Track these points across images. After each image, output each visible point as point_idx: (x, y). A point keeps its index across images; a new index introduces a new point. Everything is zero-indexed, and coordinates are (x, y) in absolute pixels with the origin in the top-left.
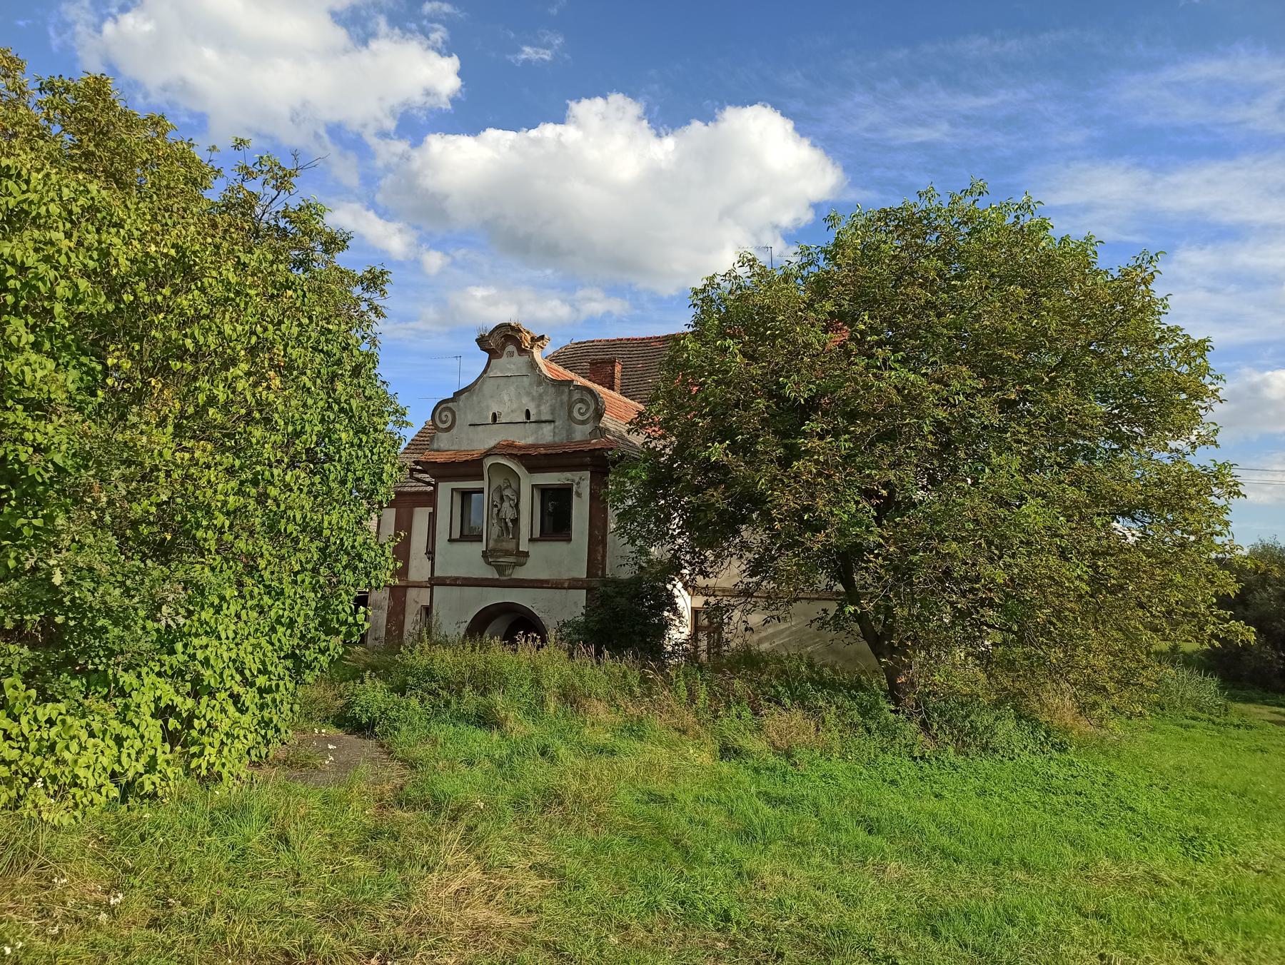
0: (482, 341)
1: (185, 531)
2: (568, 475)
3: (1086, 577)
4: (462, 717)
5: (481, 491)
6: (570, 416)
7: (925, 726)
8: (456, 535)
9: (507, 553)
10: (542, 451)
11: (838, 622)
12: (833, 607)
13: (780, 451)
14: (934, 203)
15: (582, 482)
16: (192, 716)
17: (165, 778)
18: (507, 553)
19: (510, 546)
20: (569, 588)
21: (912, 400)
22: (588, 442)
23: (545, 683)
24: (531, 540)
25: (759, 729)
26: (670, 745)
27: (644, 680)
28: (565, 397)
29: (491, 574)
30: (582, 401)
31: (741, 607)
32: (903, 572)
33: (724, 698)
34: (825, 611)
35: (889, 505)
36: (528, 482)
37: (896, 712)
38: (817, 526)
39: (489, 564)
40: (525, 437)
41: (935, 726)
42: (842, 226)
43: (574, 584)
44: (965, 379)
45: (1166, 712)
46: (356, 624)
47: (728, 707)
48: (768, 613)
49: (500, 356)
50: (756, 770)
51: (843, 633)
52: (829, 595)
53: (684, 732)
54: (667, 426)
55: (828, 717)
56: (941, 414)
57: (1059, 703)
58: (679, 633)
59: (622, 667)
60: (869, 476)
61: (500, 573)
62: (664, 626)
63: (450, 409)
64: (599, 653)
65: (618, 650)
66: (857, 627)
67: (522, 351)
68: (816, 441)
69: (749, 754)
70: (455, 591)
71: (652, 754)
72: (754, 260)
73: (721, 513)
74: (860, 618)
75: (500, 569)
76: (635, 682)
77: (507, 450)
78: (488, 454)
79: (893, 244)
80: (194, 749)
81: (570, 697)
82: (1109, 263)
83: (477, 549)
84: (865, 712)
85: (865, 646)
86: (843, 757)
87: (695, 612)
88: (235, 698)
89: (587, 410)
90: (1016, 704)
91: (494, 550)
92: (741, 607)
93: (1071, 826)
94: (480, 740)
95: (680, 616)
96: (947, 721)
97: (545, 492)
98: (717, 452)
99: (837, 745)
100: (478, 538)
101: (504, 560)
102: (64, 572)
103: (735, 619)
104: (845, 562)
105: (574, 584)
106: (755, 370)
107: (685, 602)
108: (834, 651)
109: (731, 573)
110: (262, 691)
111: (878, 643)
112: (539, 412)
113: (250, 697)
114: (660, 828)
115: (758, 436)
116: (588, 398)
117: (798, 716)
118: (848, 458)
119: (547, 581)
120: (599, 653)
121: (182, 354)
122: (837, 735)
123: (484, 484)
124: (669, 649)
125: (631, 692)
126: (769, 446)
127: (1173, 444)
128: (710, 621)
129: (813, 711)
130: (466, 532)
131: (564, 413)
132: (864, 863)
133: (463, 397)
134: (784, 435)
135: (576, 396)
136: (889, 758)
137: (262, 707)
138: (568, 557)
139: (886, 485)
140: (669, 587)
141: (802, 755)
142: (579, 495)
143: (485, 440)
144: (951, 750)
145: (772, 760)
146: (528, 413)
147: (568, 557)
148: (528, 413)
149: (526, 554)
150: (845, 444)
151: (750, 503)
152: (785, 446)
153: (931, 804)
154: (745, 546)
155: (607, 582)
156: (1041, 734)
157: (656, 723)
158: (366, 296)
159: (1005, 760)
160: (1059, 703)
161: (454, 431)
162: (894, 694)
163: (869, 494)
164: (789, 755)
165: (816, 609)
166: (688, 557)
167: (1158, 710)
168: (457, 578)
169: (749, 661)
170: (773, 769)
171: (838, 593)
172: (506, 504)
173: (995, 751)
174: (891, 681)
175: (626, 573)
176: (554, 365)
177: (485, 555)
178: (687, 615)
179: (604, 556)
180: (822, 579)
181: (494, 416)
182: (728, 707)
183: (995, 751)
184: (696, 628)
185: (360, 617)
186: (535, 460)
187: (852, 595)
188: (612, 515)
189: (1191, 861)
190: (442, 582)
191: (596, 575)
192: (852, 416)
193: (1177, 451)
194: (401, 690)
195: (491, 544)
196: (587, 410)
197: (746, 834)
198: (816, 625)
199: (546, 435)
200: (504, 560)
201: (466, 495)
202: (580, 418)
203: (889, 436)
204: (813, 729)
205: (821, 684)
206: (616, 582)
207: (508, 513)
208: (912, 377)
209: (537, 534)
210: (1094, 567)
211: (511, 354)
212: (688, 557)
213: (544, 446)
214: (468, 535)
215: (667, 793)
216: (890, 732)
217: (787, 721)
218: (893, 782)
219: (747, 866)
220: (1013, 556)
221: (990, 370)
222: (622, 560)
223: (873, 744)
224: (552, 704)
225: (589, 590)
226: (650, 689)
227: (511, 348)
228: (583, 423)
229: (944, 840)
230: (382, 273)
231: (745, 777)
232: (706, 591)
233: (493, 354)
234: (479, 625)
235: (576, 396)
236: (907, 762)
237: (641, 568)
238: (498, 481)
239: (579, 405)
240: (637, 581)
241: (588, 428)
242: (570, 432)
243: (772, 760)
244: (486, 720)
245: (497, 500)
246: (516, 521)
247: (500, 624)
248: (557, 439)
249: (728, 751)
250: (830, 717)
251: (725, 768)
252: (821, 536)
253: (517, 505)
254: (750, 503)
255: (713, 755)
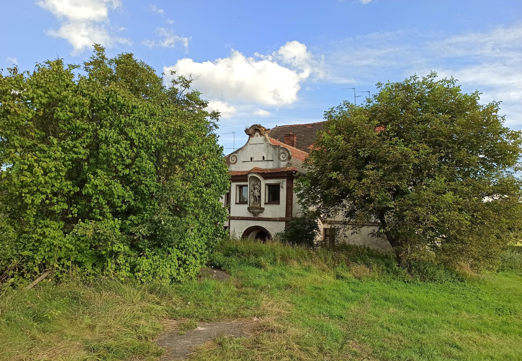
0: (247, 131)
1: (183, 209)
2: (279, 180)
3: (469, 219)
4: (251, 264)
5: (247, 186)
6: (279, 159)
7: (409, 271)
8: (238, 201)
9: (257, 208)
10: (269, 171)
11: (379, 235)
12: (376, 229)
13: (357, 175)
14: (417, 80)
15: (284, 184)
16: (185, 260)
17: (182, 277)
18: (257, 208)
19: (258, 206)
20: (279, 221)
21: (406, 156)
22: (286, 168)
23: (277, 254)
24: (265, 204)
25: (349, 270)
26: (320, 275)
27: (309, 254)
28: (277, 152)
29: (250, 215)
30: (283, 153)
31: (343, 229)
32: (401, 217)
33: (336, 261)
34: (374, 230)
35: (398, 193)
36: (264, 183)
37: (399, 266)
38: (371, 201)
39: (250, 212)
40: (263, 166)
41: (413, 271)
42: (383, 87)
43: (281, 220)
44: (425, 148)
45: (514, 270)
46: (225, 234)
47: (338, 263)
48: (352, 231)
49: (253, 137)
50: (348, 283)
51: (380, 238)
52: (375, 224)
53: (324, 271)
54: (316, 164)
55: (374, 267)
56: (417, 162)
57: (464, 266)
58: (319, 238)
59: (302, 248)
60: (390, 184)
61: (254, 215)
62: (314, 235)
63: (235, 156)
64: (293, 243)
65: (299, 243)
66: (385, 236)
67: (261, 135)
68: (371, 172)
69: (346, 278)
70: (238, 222)
71: (314, 275)
72: (349, 103)
73: (336, 196)
74: (386, 233)
75: (254, 214)
76: (306, 254)
77: (257, 171)
78: (249, 172)
79: (402, 95)
80: (187, 270)
81: (285, 259)
82: (483, 101)
83: (246, 207)
84: (387, 265)
85: (388, 243)
86: (379, 280)
87: (325, 230)
88: (194, 256)
89: (285, 156)
90: (447, 266)
91: (252, 207)
92: (343, 229)
93: (455, 302)
94: (262, 272)
95: (319, 231)
96: (419, 271)
97: (269, 186)
98: (334, 175)
99: (377, 276)
100: (246, 203)
101: (256, 212)
102: (164, 221)
103: (341, 233)
104: (381, 213)
105: (281, 220)
106: (349, 146)
107: (321, 226)
108: (378, 245)
109: (340, 216)
110: (201, 254)
111: (393, 242)
112: (268, 157)
113: (198, 255)
114: (320, 295)
115: (349, 169)
116: (286, 152)
117: (363, 267)
118: (382, 178)
119: (271, 218)
120: (293, 243)
121: (181, 156)
122: (377, 273)
123: (248, 183)
124: (316, 243)
125: (305, 258)
126: (354, 173)
127: (507, 170)
128: (330, 234)
129: (368, 265)
130: (241, 201)
131: (277, 158)
132: (383, 308)
133: (240, 152)
134: (358, 168)
135: (281, 151)
136: (396, 281)
137: (201, 258)
138: (278, 210)
139: (396, 186)
140: (316, 221)
141: (364, 279)
142: (282, 187)
143: (247, 167)
144: (418, 279)
145: (354, 280)
146: (263, 157)
147: (278, 210)
148: (263, 157)
149: (263, 209)
150: (381, 173)
151: (346, 193)
152: (360, 172)
153: (410, 295)
154: (344, 206)
155: (293, 219)
156: (454, 275)
157: (314, 267)
158: (212, 121)
159: (439, 284)
160: (464, 266)
161: (237, 164)
162: (398, 260)
163: (390, 190)
164: (360, 279)
165: (371, 229)
166: (323, 210)
167: (510, 269)
168: (239, 217)
169: (345, 247)
170: (355, 283)
171: (379, 223)
172: (256, 191)
173: (435, 280)
174: (398, 255)
175: (299, 216)
176: (272, 139)
177: (249, 209)
178: (322, 230)
179: (292, 210)
180: (373, 219)
181: (251, 159)
182: (338, 263)
183: (435, 280)
184: (326, 236)
185: (226, 232)
186: (266, 175)
187: (383, 224)
188: (295, 195)
189: (497, 315)
190: (233, 218)
191: (289, 217)
192: (384, 162)
193: (509, 172)
194: (227, 255)
195: (251, 205)
196: (285, 156)
197: (347, 299)
198: (370, 235)
199: (270, 166)
200: (256, 212)
201: (241, 187)
202: (283, 159)
203: (397, 169)
204: (368, 271)
205: (371, 256)
206: (296, 219)
207: (257, 193)
208: (406, 149)
209: (267, 201)
210: (473, 216)
211: (257, 136)
212: (323, 210)
213: (270, 170)
214: (242, 201)
215: (321, 287)
216: (397, 273)
217: (360, 268)
218: (396, 288)
219: (346, 306)
220: (442, 212)
221: (435, 145)
222: (298, 210)
223: (389, 277)
224: (279, 261)
225: (287, 222)
226: (33, 346)
227: (257, 133)
228: (284, 161)
229: (410, 304)
230: (218, 113)
231: (345, 284)
232: (330, 223)
233: (251, 135)
234: (247, 232)
235: (281, 151)
236: (402, 283)
237: (305, 214)
238: (252, 183)
239: (282, 155)
240: (303, 218)
241: (286, 163)
242: (279, 164)
243: (354, 280)
244: (259, 265)
245: (253, 189)
246: (260, 197)
247: (253, 234)
248: (274, 167)
249: (338, 277)
250: (375, 267)
251: (338, 281)
252: (372, 205)
253: (260, 191)
254: (346, 193)
255: (334, 278)
